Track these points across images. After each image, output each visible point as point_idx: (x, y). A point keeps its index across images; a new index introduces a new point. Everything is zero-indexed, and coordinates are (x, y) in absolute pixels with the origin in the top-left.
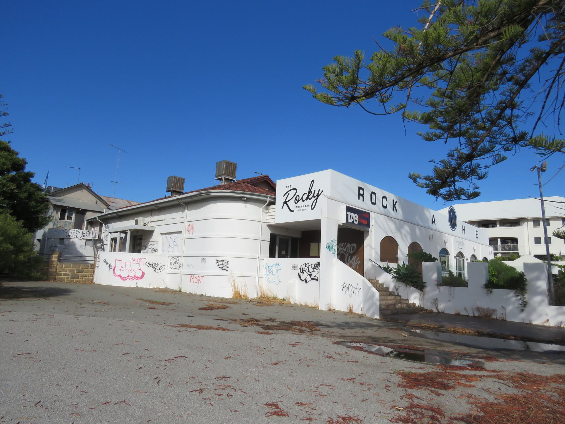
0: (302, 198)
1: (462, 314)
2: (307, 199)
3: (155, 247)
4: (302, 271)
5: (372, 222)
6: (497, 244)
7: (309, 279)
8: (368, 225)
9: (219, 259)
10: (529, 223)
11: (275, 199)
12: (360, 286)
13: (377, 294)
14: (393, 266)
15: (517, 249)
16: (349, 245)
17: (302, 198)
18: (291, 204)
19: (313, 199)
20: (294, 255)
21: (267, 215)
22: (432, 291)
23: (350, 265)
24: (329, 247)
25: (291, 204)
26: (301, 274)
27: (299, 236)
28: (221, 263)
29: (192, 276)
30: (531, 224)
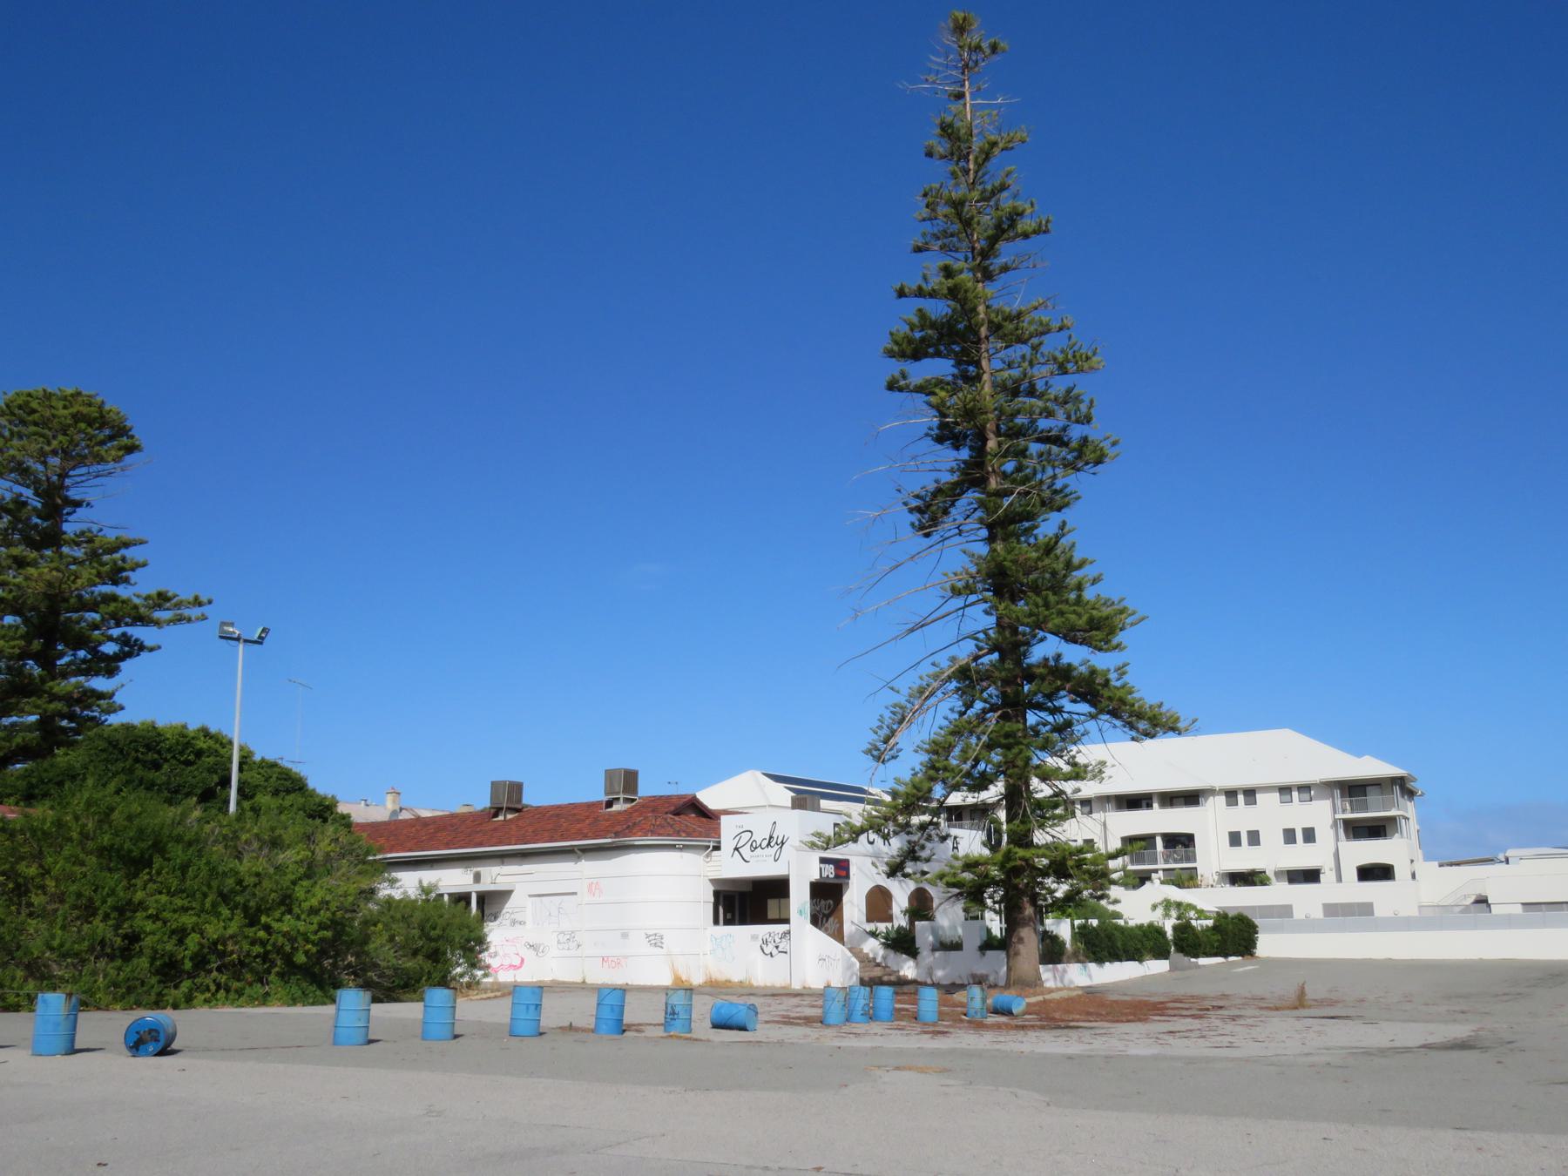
0: (760, 845)
1: (957, 982)
2: (767, 846)
3: (518, 917)
4: (766, 942)
5: (853, 870)
6: (1155, 848)
7: (775, 952)
8: (848, 876)
9: (650, 932)
10: (1217, 798)
11: (719, 842)
12: (839, 956)
13: (858, 964)
14: (882, 927)
15: (1195, 861)
16: (823, 902)
17: (760, 845)
18: (745, 851)
19: (777, 847)
20: (743, 922)
21: (709, 864)
22: (926, 956)
23: (826, 931)
24: (801, 912)
25: (745, 851)
26: (764, 946)
27: (749, 889)
28: (653, 937)
29: (606, 959)
30: (1222, 799)
